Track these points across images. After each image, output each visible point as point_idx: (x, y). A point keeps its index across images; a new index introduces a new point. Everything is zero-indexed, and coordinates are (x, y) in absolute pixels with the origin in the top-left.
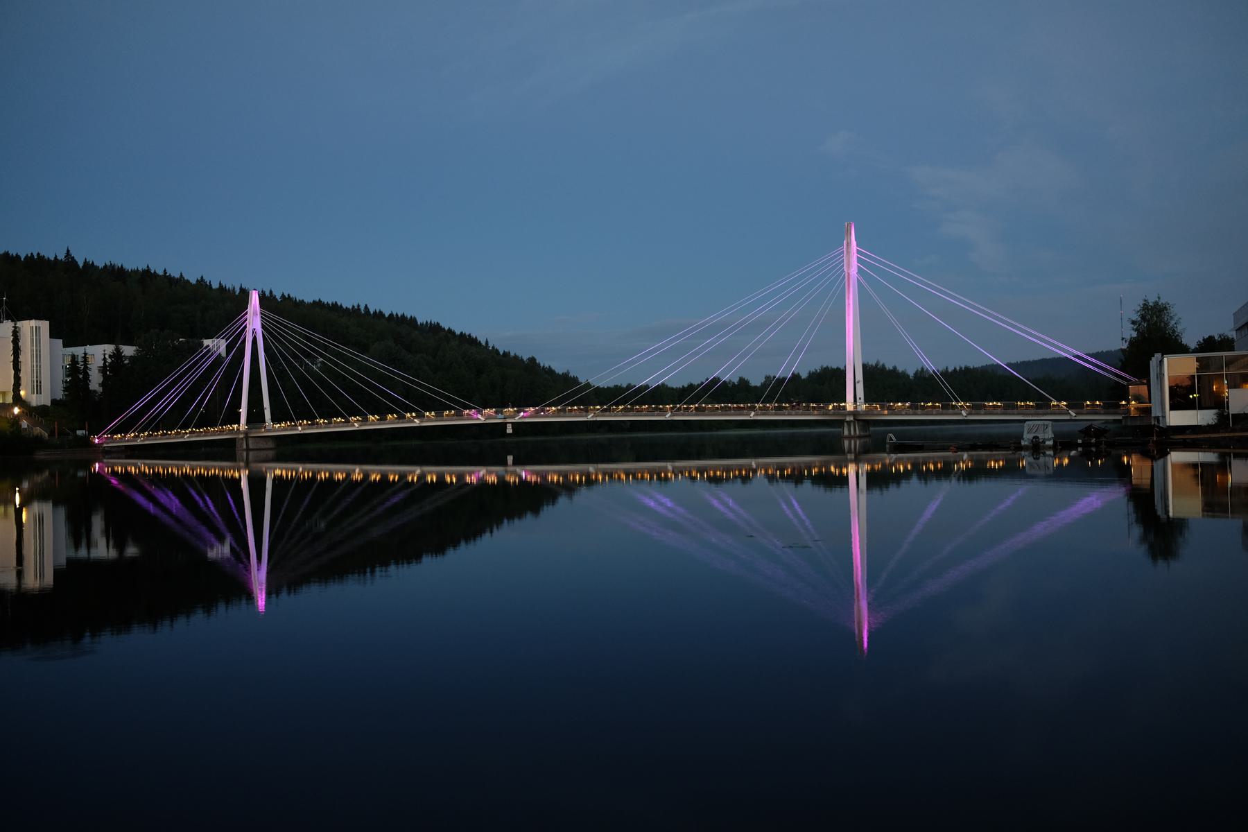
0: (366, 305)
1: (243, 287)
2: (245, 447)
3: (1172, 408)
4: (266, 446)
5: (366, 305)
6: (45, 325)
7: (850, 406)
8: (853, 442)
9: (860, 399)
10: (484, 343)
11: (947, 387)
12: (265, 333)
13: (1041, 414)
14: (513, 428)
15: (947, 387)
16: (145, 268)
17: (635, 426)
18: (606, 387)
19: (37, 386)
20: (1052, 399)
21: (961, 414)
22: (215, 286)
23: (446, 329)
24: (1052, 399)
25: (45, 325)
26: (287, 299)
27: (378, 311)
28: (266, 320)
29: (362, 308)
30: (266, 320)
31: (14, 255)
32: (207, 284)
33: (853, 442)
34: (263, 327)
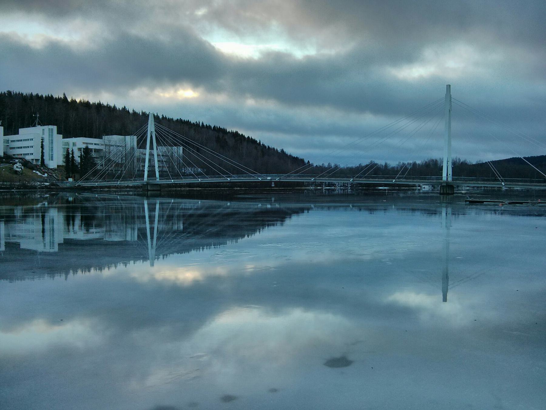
0: (202, 122)
1: (210, 125)
2: (146, 189)
3: (442, 180)
4: (157, 189)
5: (202, 122)
6: (55, 128)
7: (444, 179)
8: (445, 192)
9: (450, 174)
10: (258, 142)
11: (497, 173)
12: (157, 134)
13: (324, 180)
14: (275, 184)
15: (497, 173)
16: (98, 102)
17: (176, 185)
18: (345, 168)
19: (51, 157)
20: (523, 159)
21: (199, 180)
22: (131, 111)
23: (241, 134)
24: (523, 159)
25: (55, 128)
26: (164, 118)
27: (21, 93)
28: (157, 127)
29: (201, 124)
30: (157, 127)
31: (218, 127)
32: (127, 110)
33: (445, 192)
34: (156, 131)
